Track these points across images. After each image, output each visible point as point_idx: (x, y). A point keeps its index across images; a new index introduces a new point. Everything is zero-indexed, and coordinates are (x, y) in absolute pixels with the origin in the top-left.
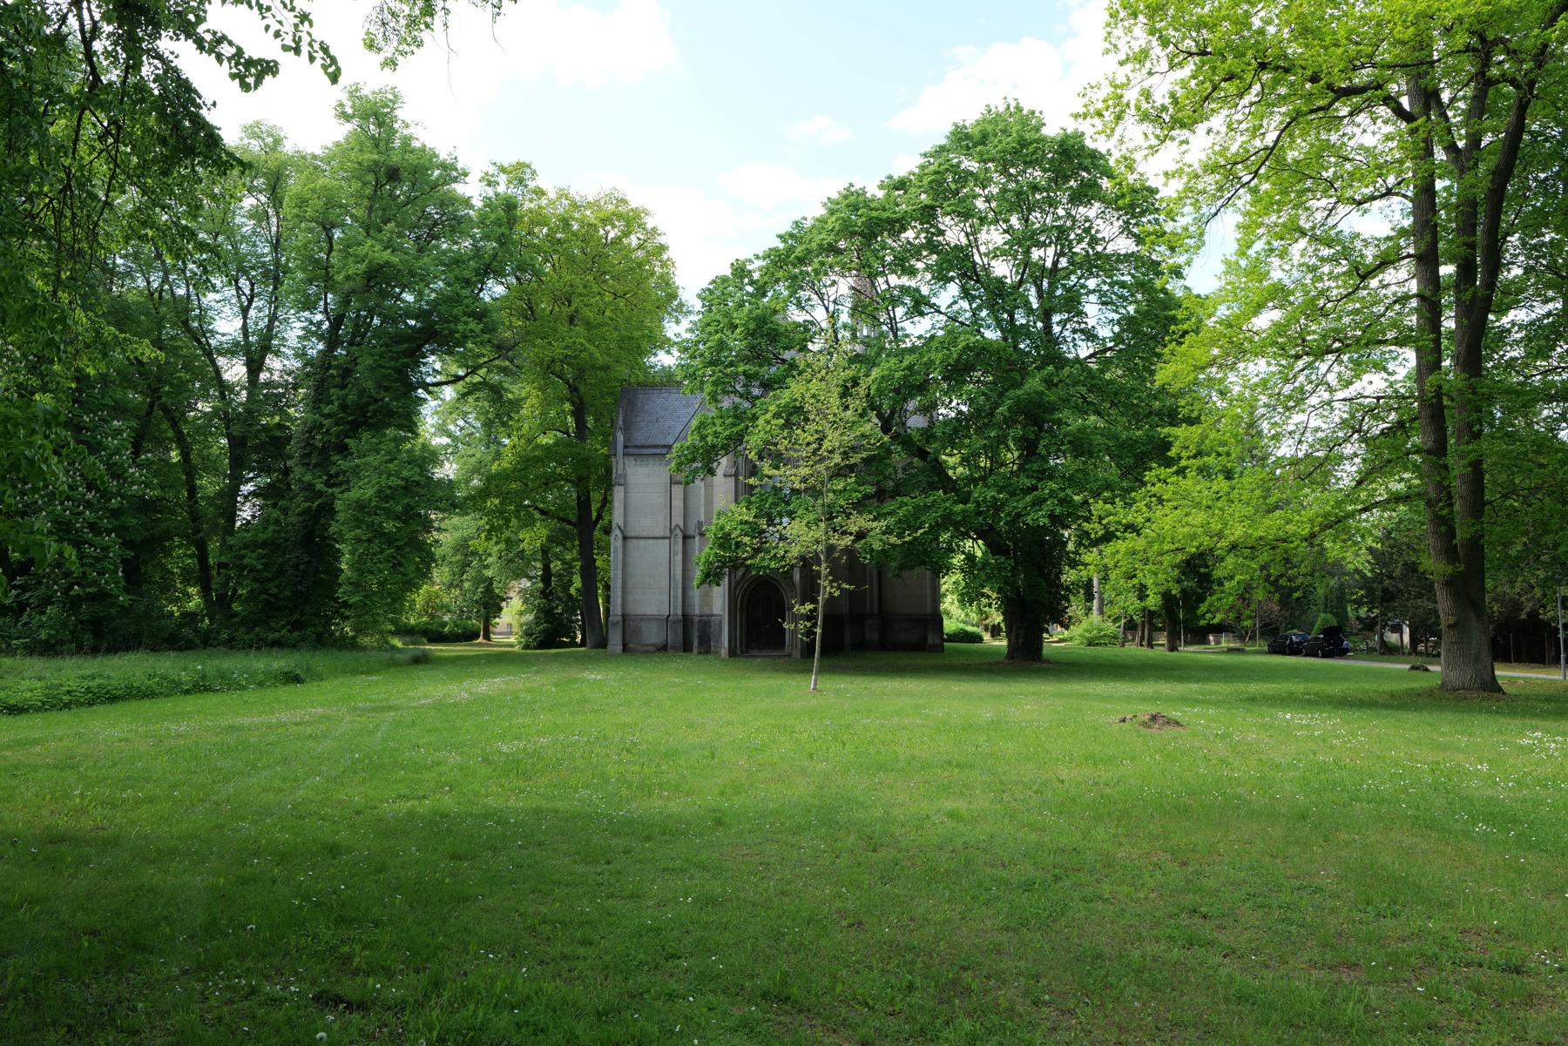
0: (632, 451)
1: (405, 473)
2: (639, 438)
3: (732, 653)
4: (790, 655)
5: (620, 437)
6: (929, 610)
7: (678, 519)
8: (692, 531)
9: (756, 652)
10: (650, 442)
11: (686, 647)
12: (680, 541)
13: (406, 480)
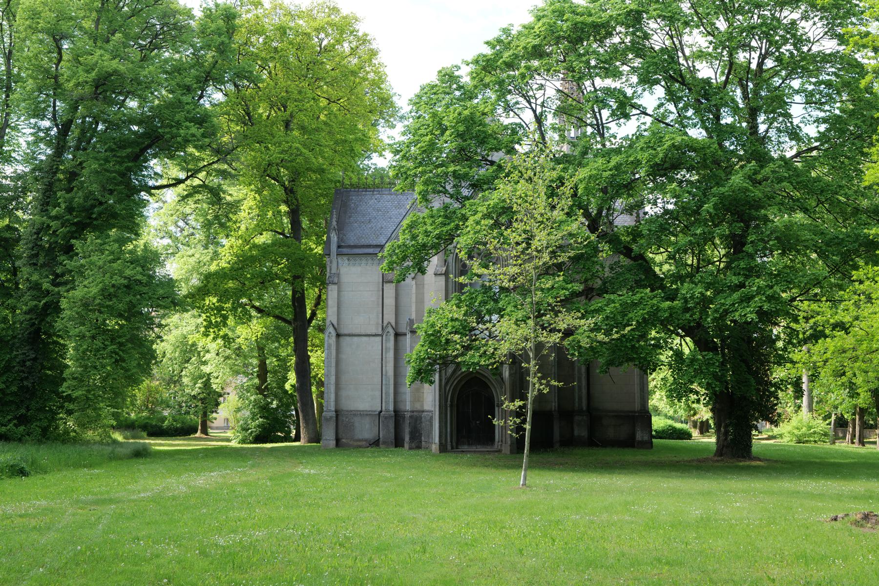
0: (345, 250)
1: (128, 272)
2: (352, 238)
3: (443, 449)
4: (499, 451)
5: (334, 238)
6: (637, 407)
7: (390, 317)
8: (403, 329)
9: (465, 448)
10: (363, 242)
11: (398, 443)
12: (334, 338)
13: (128, 278)
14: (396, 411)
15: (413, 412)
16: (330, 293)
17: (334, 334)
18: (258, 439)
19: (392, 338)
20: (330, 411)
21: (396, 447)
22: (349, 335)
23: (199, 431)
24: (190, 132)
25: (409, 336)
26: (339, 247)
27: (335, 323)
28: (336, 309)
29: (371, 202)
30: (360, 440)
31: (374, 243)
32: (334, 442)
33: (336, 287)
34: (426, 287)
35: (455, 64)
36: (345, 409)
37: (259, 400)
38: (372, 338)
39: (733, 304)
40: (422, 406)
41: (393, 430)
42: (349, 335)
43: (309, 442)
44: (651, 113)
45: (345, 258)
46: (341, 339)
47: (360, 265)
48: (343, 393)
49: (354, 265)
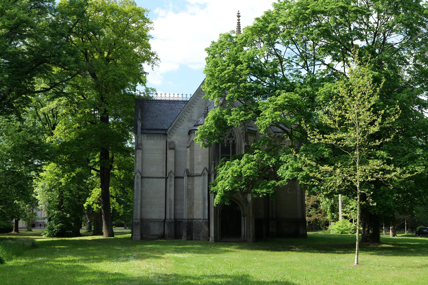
0: (145, 131)
2: (148, 125)
4: (246, 241)
7: (171, 168)
8: (181, 173)
10: (154, 127)
12: (140, 179)
14: (141, 219)
15: (188, 219)
16: (137, 154)
17: (140, 177)
18: (58, 235)
19: (173, 179)
20: (137, 219)
21: (176, 238)
22: (147, 178)
23: (14, 230)
24: (67, 59)
25: (186, 178)
26: (142, 129)
27: (140, 170)
28: (141, 163)
29: (156, 106)
30: (153, 235)
31: (161, 128)
32: (140, 237)
33: (140, 151)
34: (195, 152)
35: (233, 30)
36: (144, 218)
37: (59, 213)
38: (160, 180)
39: (406, 162)
40: (193, 216)
41: (173, 230)
42: (147, 178)
43: (109, 236)
44: (285, 74)
45: (145, 135)
46: (143, 179)
47: (153, 139)
48: (178, 207)
49: (150, 139)
